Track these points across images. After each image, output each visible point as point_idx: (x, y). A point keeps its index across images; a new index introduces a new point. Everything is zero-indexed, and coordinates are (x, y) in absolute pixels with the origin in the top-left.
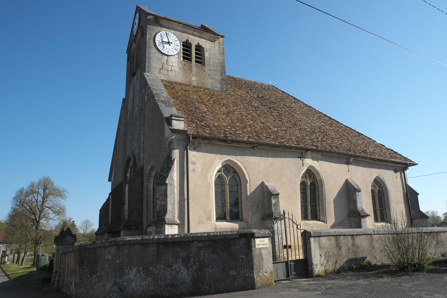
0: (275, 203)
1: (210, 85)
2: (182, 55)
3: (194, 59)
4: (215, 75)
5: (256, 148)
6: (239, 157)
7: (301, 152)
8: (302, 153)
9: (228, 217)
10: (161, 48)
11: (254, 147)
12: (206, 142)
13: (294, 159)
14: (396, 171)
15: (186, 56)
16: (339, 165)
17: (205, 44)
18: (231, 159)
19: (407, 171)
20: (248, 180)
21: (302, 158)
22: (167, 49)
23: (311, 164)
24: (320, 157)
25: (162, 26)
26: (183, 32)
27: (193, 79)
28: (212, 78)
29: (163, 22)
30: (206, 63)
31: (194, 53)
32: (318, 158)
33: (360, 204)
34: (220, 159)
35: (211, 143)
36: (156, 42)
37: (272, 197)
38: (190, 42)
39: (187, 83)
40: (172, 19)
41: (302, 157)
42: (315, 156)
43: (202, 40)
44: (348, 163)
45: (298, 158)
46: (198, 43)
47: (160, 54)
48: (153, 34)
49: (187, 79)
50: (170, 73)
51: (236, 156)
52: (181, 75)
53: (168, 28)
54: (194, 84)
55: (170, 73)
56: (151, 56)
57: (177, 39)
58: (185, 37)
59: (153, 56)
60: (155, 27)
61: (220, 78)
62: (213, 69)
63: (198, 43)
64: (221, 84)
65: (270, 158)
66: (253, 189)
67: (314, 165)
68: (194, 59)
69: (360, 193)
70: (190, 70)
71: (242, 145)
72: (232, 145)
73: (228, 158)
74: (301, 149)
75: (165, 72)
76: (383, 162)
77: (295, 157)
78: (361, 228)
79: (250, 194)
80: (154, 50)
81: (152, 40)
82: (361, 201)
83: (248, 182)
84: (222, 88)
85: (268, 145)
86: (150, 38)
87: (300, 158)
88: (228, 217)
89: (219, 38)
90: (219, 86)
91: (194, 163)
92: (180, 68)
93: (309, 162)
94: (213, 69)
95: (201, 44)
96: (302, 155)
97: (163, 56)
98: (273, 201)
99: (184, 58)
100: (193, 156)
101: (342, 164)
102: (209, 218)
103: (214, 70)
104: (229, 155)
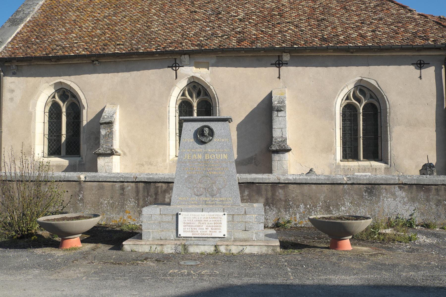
0: (106, 135)
5: (97, 62)
6: (73, 78)
7: (171, 58)
8: (175, 59)
9: (63, 151)
11: (93, 61)
12: (26, 64)
13: (162, 69)
14: (420, 65)
16: (257, 69)
18: (62, 80)
20: (85, 106)
21: (176, 67)
23: (193, 75)
24: (213, 61)
32: (208, 63)
33: (279, 130)
34: (47, 82)
35: (32, 64)
37: (102, 126)
41: (175, 65)
42: (201, 60)
44: (279, 64)
45: (169, 67)
51: (70, 76)
65: (120, 74)
66: (91, 117)
67: (198, 75)
69: (280, 114)
71: (75, 61)
72: (60, 63)
73: (59, 81)
74: (172, 53)
76: (375, 52)
77: (163, 67)
78: (270, 171)
79: (87, 123)
82: (282, 126)
83: (84, 108)
85: (114, 55)
87: (172, 67)
88: (63, 151)
91: (12, 91)
93: (189, 71)
96: (176, 63)
98: (103, 132)
100: (11, 83)
101: (266, 66)
102: (330, 148)
104: (60, 76)
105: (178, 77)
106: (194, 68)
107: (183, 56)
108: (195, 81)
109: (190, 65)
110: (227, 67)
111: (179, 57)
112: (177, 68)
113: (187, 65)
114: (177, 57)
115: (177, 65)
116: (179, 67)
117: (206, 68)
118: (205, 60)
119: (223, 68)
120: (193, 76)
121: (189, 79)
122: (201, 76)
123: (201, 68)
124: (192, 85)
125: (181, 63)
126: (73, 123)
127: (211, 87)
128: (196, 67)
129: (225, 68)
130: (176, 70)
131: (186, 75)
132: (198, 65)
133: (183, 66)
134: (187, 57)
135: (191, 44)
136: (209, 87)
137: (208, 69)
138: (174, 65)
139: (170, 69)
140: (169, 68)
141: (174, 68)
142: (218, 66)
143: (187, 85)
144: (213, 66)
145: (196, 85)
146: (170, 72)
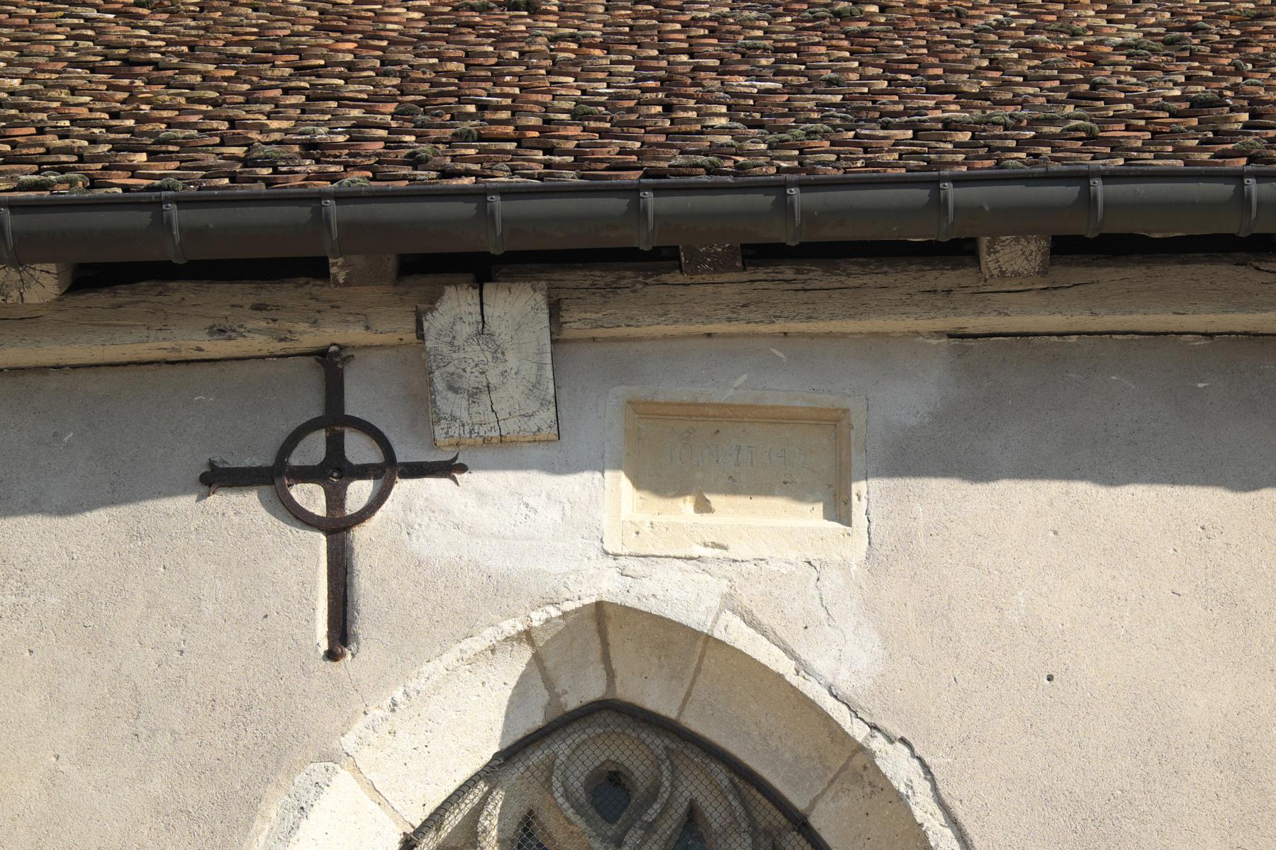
8: (331, 364)
13: (100, 516)
21: (335, 472)
23: (606, 585)
24: (907, 396)
41: (324, 456)
42: (733, 386)
45: (218, 478)
67: (684, 597)
77: (119, 486)
87: (270, 478)
96: (334, 419)
105: (363, 626)
106: (611, 499)
107: (456, 308)
108: (628, 691)
109: (553, 450)
110: (1109, 479)
111: (392, 328)
112: (359, 492)
113: (505, 450)
114: (361, 327)
115: (359, 449)
116: (388, 470)
117: (795, 490)
118: (785, 389)
119: (1054, 488)
120: (600, 612)
121: (545, 654)
122: (730, 603)
123: (733, 488)
124: (578, 757)
125: (422, 405)
126: (503, 353)
127: (897, 766)
128: (658, 478)
129: (1082, 488)
130: (337, 528)
131: (499, 589)
132: (680, 454)
133: (447, 469)
134: (516, 310)
135: (923, 67)
136: (856, 768)
137: (839, 511)
138: (313, 450)
139: (246, 506)
140: (223, 501)
141: (310, 496)
142: (977, 470)
143: (508, 756)
144: (909, 458)
145: (634, 755)
146: (254, 552)
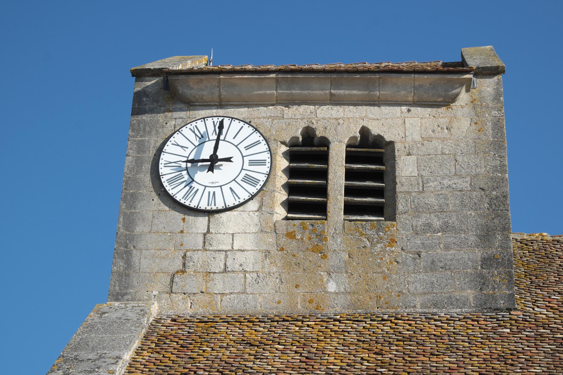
1: (418, 301)
2: (283, 196)
3: (337, 198)
4: (447, 248)
10: (178, 193)
15: (305, 194)
17: (397, 123)
19: (385, 137)
22: (208, 187)
25: (191, 104)
26: (289, 102)
27: (332, 287)
28: (432, 266)
29: (192, 88)
30: (401, 206)
31: (342, 173)
36: (163, 170)
38: (319, 133)
39: (300, 308)
40: (404, 65)
43: (386, 110)
46: (364, 131)
47: (179, 216)
48: (154, 142)
49: (300, 291)
50: (219, 285)
52: (273, 282)
53: (221, 105)
54: (337, 306)
55: (219, 285)
56: (139, 229)
57: (256, 137)
58: (295, 120)
59: (147, 229)
60: (160, 117)
61: (478, 254)
62: (437, 223)
63: (364, 131)
64: (481, 282)
68: (337, 198)
70: (317, 249)
75: (191, 283)
80: (152, 204)
81: (147, 166)
84: (487, 306)
86: (139, 162)
89: (469, 86)
90: (470, 294)
92: (267, 254)
94: (437, 223)
95: (375, 130)
97: (190, 219)
99: (291, 206)
103: (445, 228)
